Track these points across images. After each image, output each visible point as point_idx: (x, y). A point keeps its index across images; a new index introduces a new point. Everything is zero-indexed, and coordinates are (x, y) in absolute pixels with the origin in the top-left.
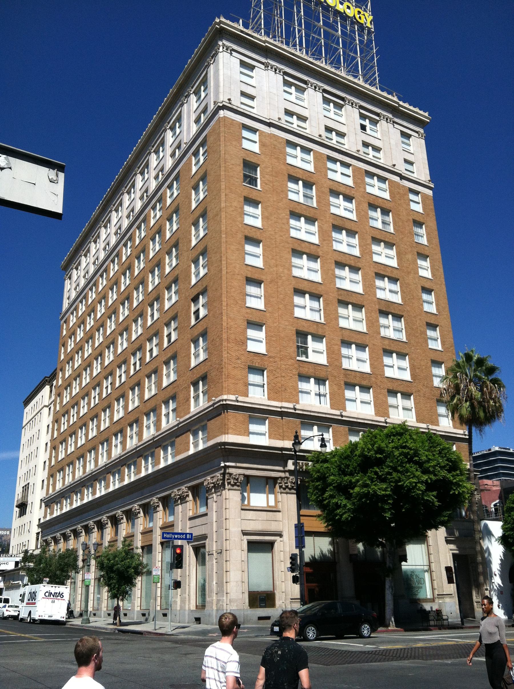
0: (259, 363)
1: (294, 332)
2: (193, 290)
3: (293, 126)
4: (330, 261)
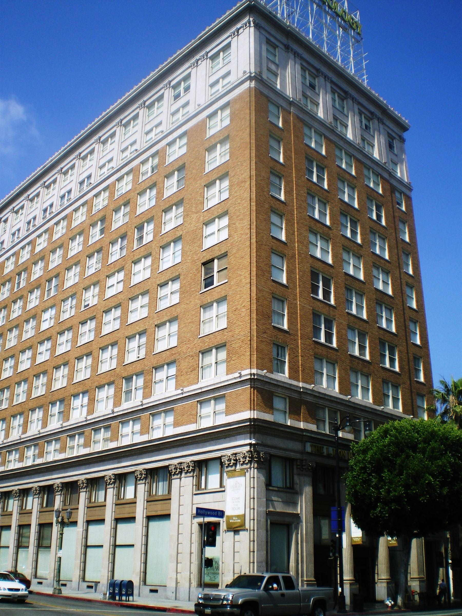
0: (282, 339)
1: (311, 312)
2: (204, 254)
3: (220, 91)
4: (338, 244)
